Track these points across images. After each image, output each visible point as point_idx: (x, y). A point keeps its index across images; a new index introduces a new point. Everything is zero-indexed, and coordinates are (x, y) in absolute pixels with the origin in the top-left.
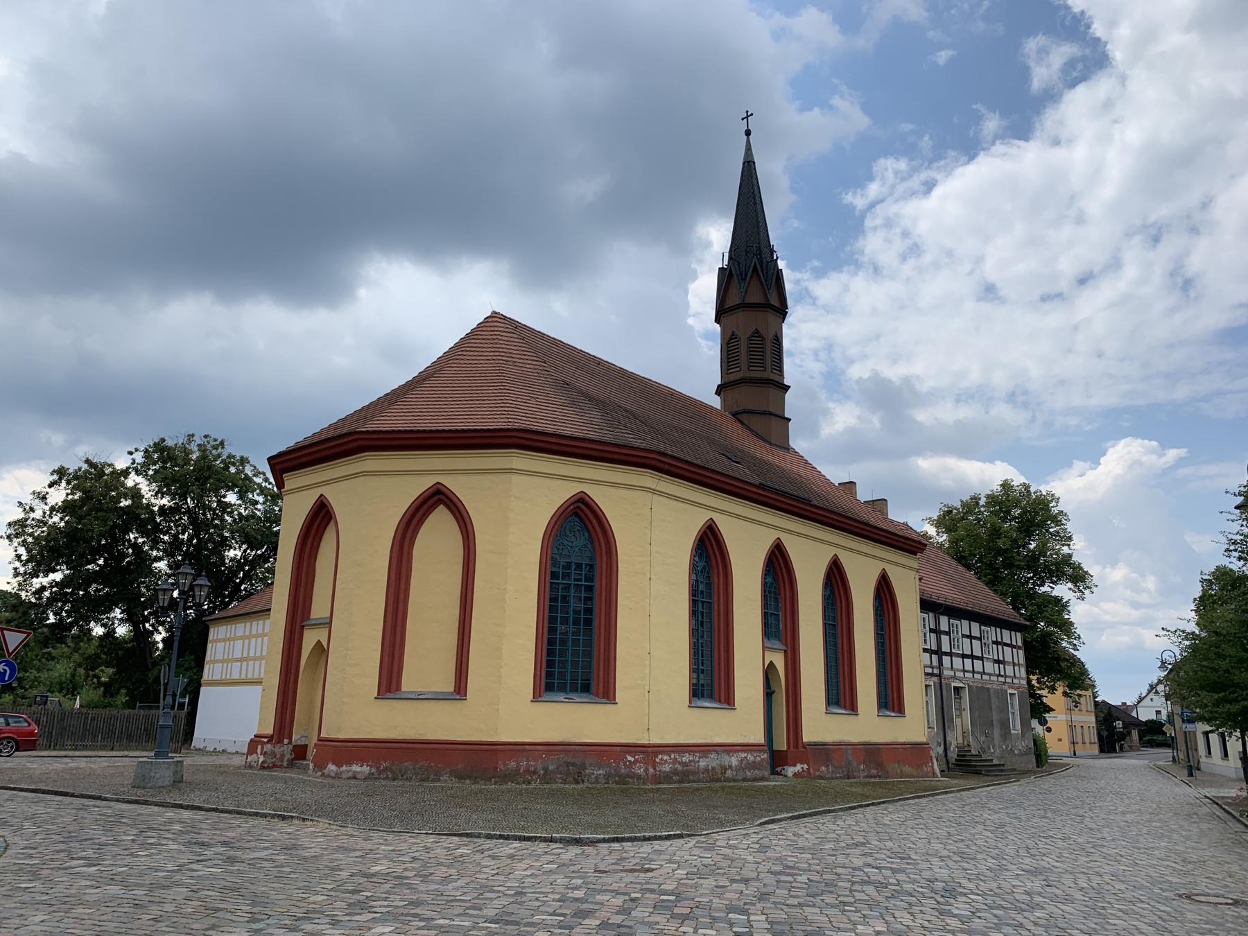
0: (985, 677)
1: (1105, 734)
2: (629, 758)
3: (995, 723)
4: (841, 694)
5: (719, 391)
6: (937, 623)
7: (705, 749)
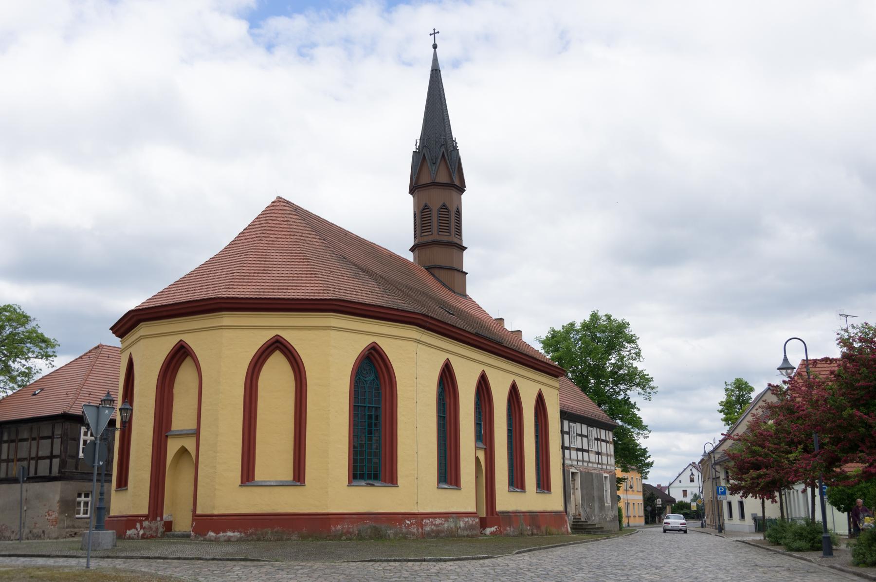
0: (590, 465)
1: (649, 509)
2: (408, 522)
5: (412, 250)
7: (446, 515)
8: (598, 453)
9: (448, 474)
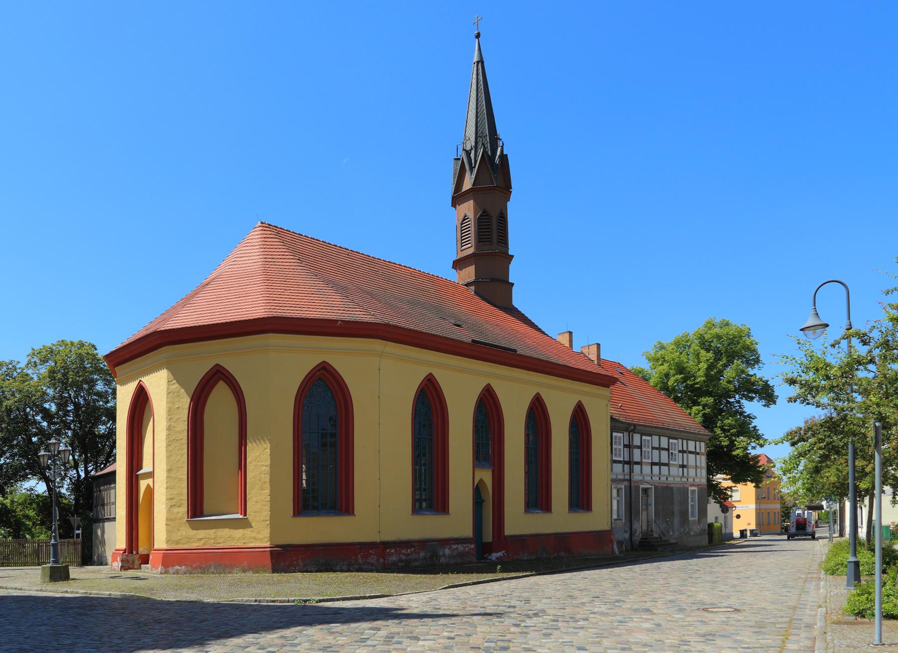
3: (676, 513)
4: (538, 498)
6: (631, 439)
8: (683, 466)
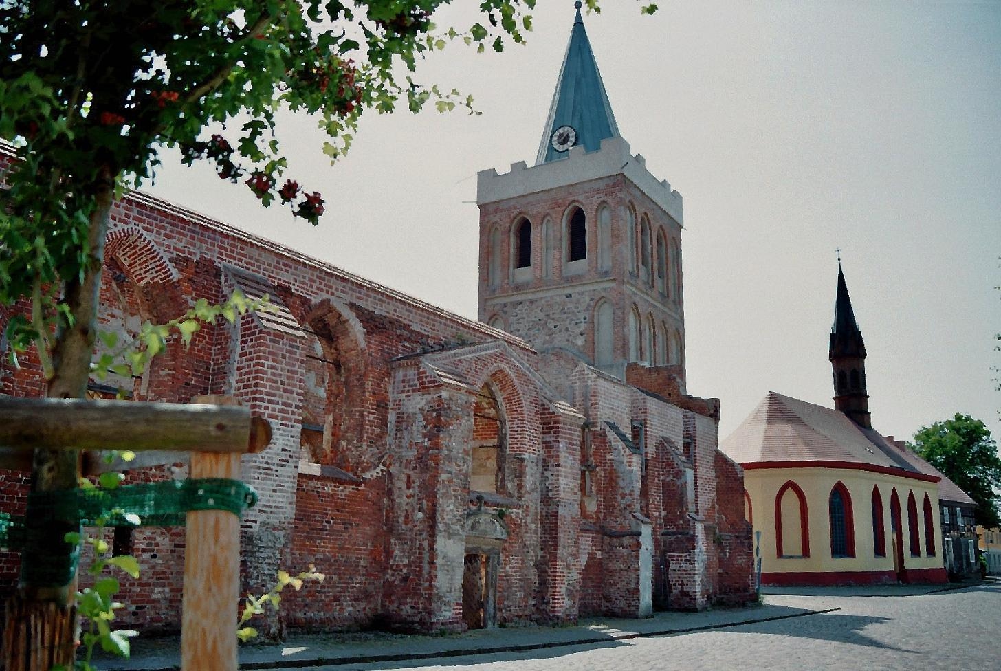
9: (880, 550)
